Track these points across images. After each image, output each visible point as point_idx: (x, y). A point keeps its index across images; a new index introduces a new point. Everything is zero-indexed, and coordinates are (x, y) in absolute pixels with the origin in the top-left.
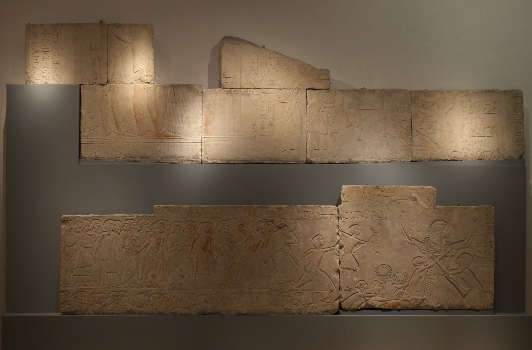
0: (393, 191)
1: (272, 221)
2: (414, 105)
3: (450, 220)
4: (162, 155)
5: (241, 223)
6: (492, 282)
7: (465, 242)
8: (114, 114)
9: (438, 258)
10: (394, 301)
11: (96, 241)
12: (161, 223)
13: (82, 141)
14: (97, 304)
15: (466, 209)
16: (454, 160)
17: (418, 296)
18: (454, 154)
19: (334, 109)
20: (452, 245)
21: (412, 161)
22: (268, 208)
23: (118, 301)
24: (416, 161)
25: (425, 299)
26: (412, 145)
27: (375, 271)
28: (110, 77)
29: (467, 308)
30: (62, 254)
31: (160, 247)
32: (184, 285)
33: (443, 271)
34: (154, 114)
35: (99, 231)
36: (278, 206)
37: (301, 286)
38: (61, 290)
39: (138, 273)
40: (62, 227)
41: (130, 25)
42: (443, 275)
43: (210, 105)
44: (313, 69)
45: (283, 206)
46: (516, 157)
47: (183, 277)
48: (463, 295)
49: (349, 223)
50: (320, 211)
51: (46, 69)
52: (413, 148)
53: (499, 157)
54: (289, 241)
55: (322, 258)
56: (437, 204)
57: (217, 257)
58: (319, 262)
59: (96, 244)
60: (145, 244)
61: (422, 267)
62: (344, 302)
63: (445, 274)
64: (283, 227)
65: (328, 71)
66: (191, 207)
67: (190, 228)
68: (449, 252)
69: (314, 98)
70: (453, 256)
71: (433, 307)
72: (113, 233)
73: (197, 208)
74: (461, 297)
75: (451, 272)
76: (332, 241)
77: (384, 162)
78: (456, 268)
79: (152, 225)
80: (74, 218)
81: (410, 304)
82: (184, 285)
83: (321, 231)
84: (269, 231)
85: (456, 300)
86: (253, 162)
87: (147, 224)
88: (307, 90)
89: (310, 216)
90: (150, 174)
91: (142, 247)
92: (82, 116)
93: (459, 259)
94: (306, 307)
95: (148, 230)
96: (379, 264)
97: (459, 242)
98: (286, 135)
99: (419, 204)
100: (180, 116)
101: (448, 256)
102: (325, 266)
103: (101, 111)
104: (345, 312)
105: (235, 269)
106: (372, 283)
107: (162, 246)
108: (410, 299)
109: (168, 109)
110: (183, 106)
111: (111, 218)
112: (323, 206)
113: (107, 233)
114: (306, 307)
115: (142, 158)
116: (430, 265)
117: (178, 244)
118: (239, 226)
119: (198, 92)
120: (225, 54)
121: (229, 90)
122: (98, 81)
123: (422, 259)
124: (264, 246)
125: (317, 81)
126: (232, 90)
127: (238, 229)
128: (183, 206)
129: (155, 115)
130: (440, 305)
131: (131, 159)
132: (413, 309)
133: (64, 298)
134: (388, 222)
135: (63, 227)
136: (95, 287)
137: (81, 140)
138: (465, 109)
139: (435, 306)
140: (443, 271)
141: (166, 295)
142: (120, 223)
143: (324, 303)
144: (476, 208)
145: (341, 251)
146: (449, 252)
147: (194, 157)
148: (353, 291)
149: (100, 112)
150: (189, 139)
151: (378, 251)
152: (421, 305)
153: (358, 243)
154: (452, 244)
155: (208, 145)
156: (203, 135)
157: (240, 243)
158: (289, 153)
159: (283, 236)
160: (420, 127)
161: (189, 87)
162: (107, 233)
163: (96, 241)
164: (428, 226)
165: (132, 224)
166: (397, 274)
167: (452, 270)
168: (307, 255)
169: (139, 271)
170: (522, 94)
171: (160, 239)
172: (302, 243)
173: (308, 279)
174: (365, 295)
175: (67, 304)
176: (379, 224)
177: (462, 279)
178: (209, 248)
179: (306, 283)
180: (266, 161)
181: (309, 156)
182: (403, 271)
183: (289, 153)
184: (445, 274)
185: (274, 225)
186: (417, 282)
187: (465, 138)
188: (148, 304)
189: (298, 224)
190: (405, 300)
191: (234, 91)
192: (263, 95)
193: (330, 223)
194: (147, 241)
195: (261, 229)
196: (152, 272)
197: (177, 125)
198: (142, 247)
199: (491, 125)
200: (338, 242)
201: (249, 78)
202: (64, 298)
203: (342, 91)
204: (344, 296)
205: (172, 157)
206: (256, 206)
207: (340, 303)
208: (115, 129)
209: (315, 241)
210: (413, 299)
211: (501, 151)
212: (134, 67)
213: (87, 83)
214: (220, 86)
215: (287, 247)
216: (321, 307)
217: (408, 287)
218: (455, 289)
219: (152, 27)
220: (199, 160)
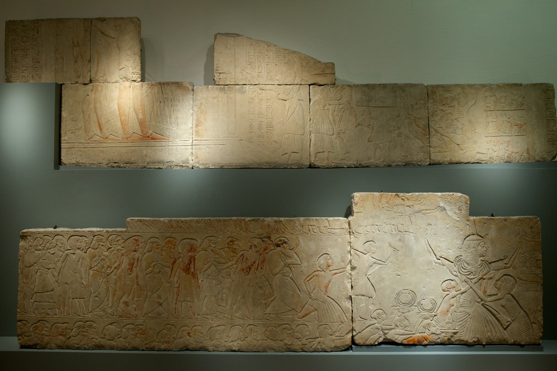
0: (417, 200)
1: (269, 238)
2: (431, 101)
3: (487, 235)
4: (148, 160)
5: (230, 239)
6: (540, 311)
7: (505, 261)
8: (97, 116)
9: (473, 281)
10: (419, 334)
11: (58, 261)
12: (134, 239)
13: (63, 145)
14: (60, 337)
15: (506, 220)
16: (478, 163)
17: (449, 329)
18: (478, 156)
19: (341, 106)
20: (490, 265)
21: (430, 164)
22: (264, 220)
23: (85, 334)
24: (434, 164)
25: (457, 332)
26: (430, 147)
27: (395, 298)
28: (93, 76)
29: (509, 342)
30: (20, 276)
31: (134, 269)
32: (163, 315)
33: (479, 298)
34: (140, 114)
35: (62, 249)
36: (276, 218)
37: (303, 317)
38: (19, 319)
39: (108, 300)
40: (21, 244)
41: (115, 19)
42: (479, 303)
43: (201, 104)
44: (317, 62)
45: (282, 219)
46: (549, 159)
47: (161, 305)
48: (505, 327)
49: (362, 239)
50: (327, 225)
51: (25, 68)
52: (431, 149)
53: (529, 159)
54: (289, 261)
55: (330, 282)
56: (471, 214)
57: (202, 281)
58: (327, 287)
59: (59, 264)
60: (116, 265)
61: (454, 293)
62: (357, 336)
63: (482, 300)
64: (282, 244)
65: (333, 64)
66: (171, 221)
67: (170, 245)
68: (486, 274)
69: (317, 94)
70: (491, 278)
71: (467, 341)
72: (78, 251)
73: (178, 222)
74: (501, 329)
75: (489, 299)
76: (343, 261)
77: (398, 165)
78: (496, 293)
79: (124, 242)
80: (34, 233)
81: (439, 338)
82: (163, 315)
83: (329, 249)
84: (265, 249)
85: (497, 333)
86: (250, 166)
87: (118, 241)
88: (310, 85)
89: (315, 231)
90: (133, 181)
91: (113, 268)
92: (62, 118)
93: (499, 282)
94: (310, 342)
95: (120, 247)
96: (401, 289)
97: (498, 261)
98: (287, 136)
99: (449, 216)
100: (169, 117)
101: (484, 279)
102: (333, 292)
103: (83, 113)
104: (359, 348)
105: (224, 296)
106: (392, 313)
107: (136, 267)
108: (438, 332)
109: (155, 109)
110: (171, 106)
111: (76, 233)
112: (331, 218)
113: (72, 251)
114: (310, 342)
115: (127, 163)
116: (463, 289)
117: (155, 265)
118: (228, 244)
119: (189, 89)
120: (218, 49)
121: (222, 86)
122: (81, 80)
123: (453, 282)
124: (259, 268)
125: (323, 76)
126: (225, 86)
127: (227, 247)
128: (162, 219)
129: (141, 116)
130: (476, 340)
131: (115, 165)
132: (441, 344)
133: (22, 329)
134: (410, 238)
135: (22, 243)
136: (58, 316)
137: (62, 145)
138: (489, 105)
139: (470, 341)
140: (479, 298)
141: (141, 327)
142: (86, 239)
143: (333, 337)
144: (518, 219)
145: (353, 273)
146: (486, 274)
147: (184, 162)
148: (368, 323)
149: (82, 114)
150: (178, 142)
151: (399, 273)
152: (453, 340)
153: (375, 263)
154: (490, 263)
155: (199, 149)
156: (196, 138)
157: (230, 264)
158: (290, 156)
159: (283, 255)
160: (438, 126)
161: (178, 85)
162: (72, 251)
163: (58, 261)
164: (459, 242)
165: (101, 240)
166: (423, 302)
167: (490, 296)
168: (311, 278)
169: (109, 297)
170: (553, 87)
171: (134, 259)
172: (305, 264)
173: (313, 308)
174: (384, 327)
175: (25, 336)
176: (400, 240)
177: (503, 306)
178: (192, 270)
179: (311, 312)
180: (264, 165)
181: (312, 160)
182: (431, 297)
183: (290, 156)
184: (482, 300)
185: (271, 242)
186: (448, 311)
187: (490, 138)
188: (121, 337)
189: (301, 240)
190: (433, 334)
191: (229, 87)
192: (260, 92)
193: (339, 240)
194: (118, 261)
195: (255, 246)
196: (124, 299)
197: (166, 127)
198: (113, 268)
199: (519, 122)
200: (351, 261)
201: (244, 73)
202: (22, 329)
203: (349, 86)
204: (357, 329)
205: (160, 162)
206: (249, 219)
207: (353, 337)
208: (98, 132)
209: (322, 261)
210: (443, 332)
211: (531, 153)
212: (119, 64)
213: (69, 82)
214: (214, 83)
215: (288, 269)
216: (329, 341)
217: (436, 317)
218: (494, 319)
219: (139, 20)
220: (189, 165)
